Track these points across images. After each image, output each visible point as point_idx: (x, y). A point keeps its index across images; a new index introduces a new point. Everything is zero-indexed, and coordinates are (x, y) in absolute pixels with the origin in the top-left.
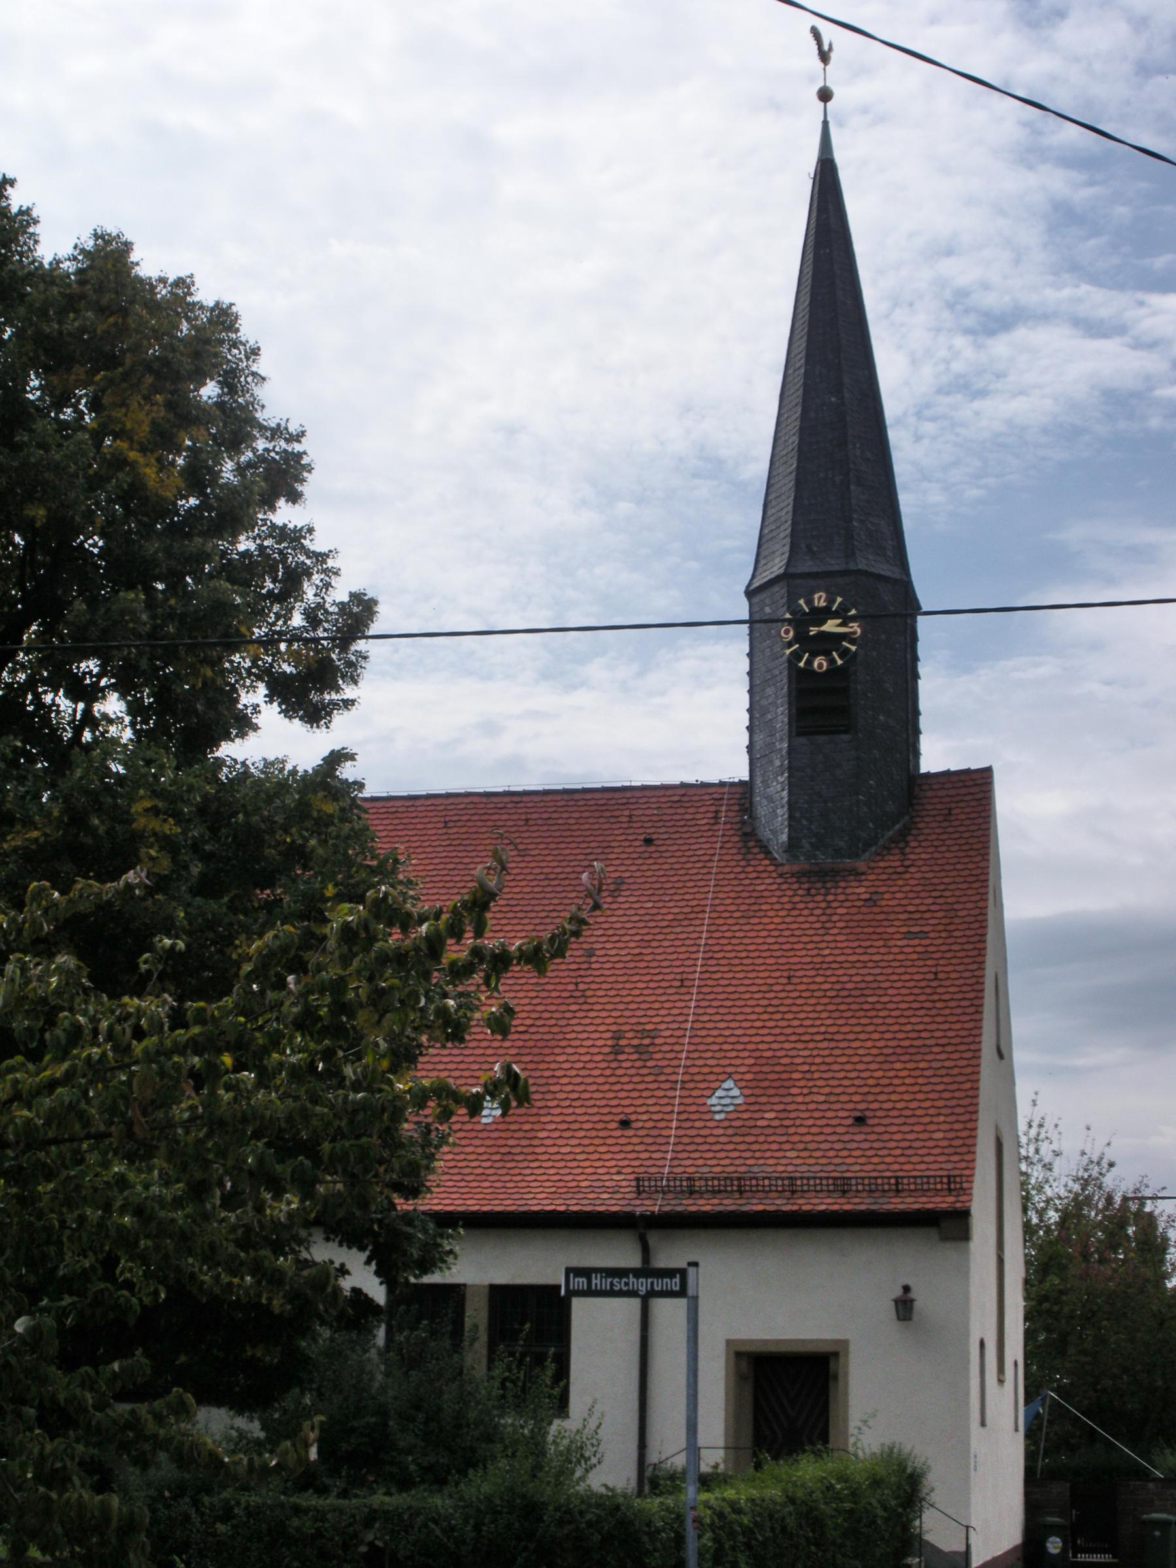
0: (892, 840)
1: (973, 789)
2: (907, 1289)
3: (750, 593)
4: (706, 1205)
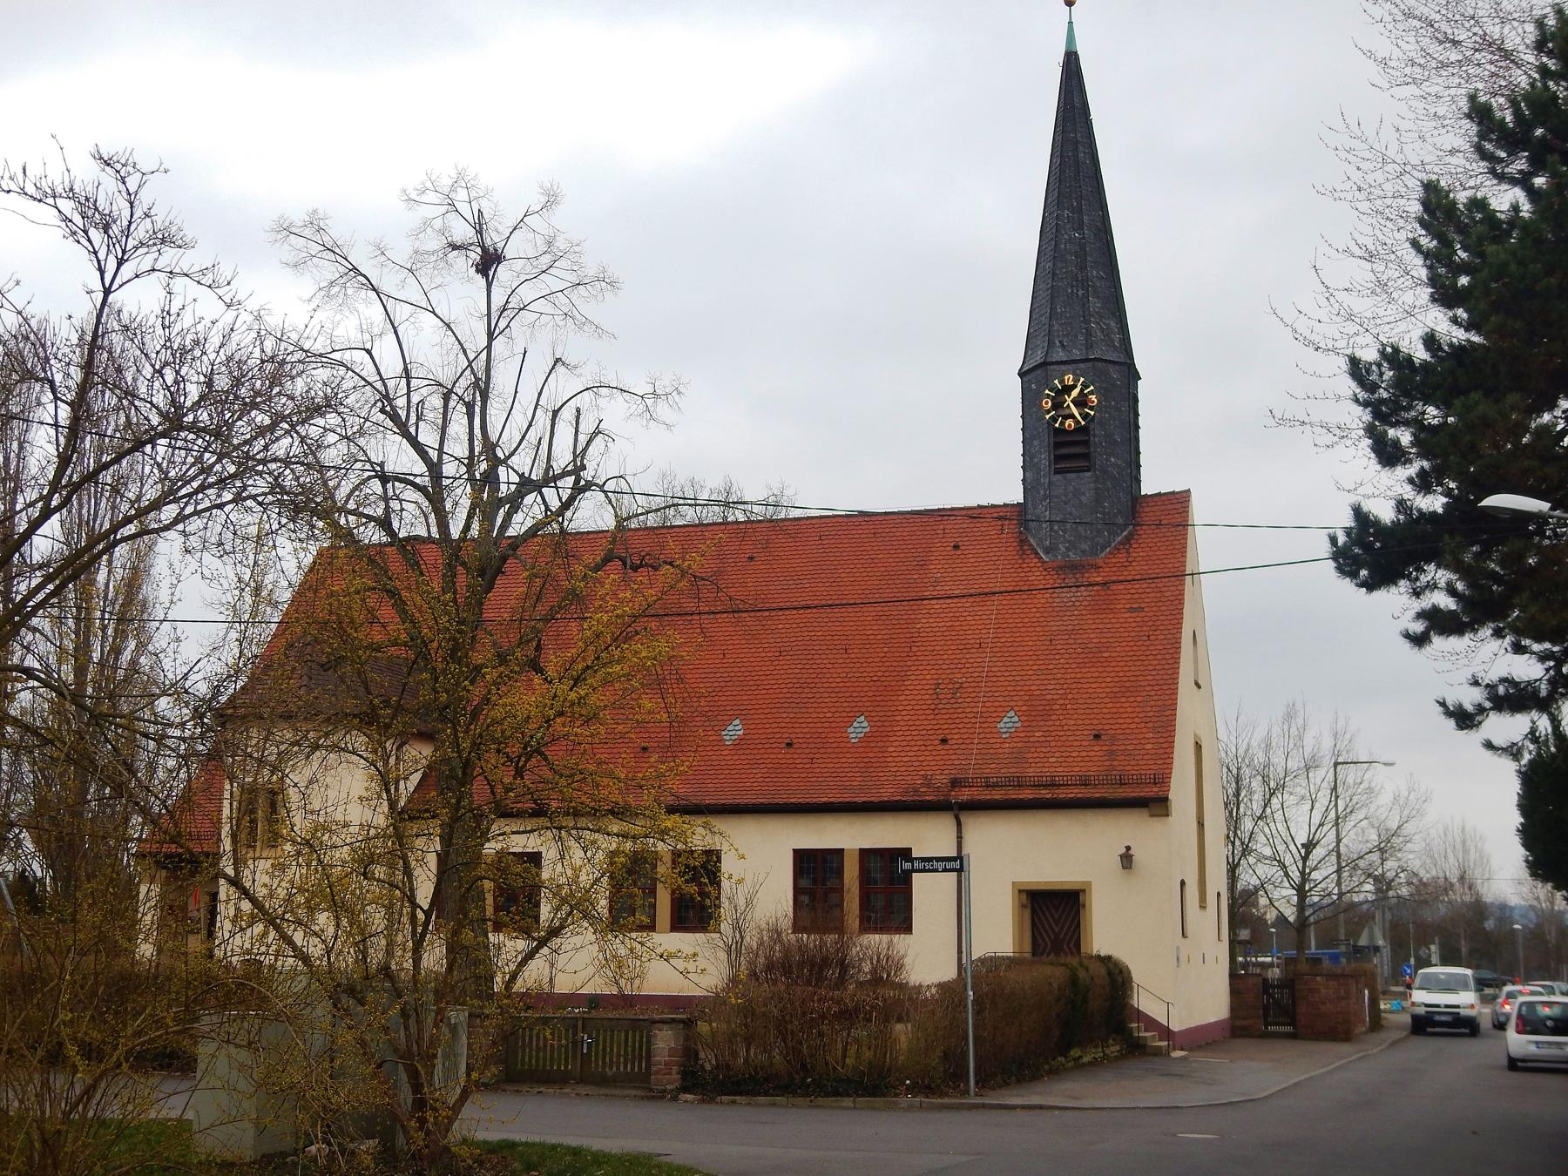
0: (1120, 543)
1: (1177, 503)
2: (1128, 848)
3: (1021, 374)
4: (997, 795)
